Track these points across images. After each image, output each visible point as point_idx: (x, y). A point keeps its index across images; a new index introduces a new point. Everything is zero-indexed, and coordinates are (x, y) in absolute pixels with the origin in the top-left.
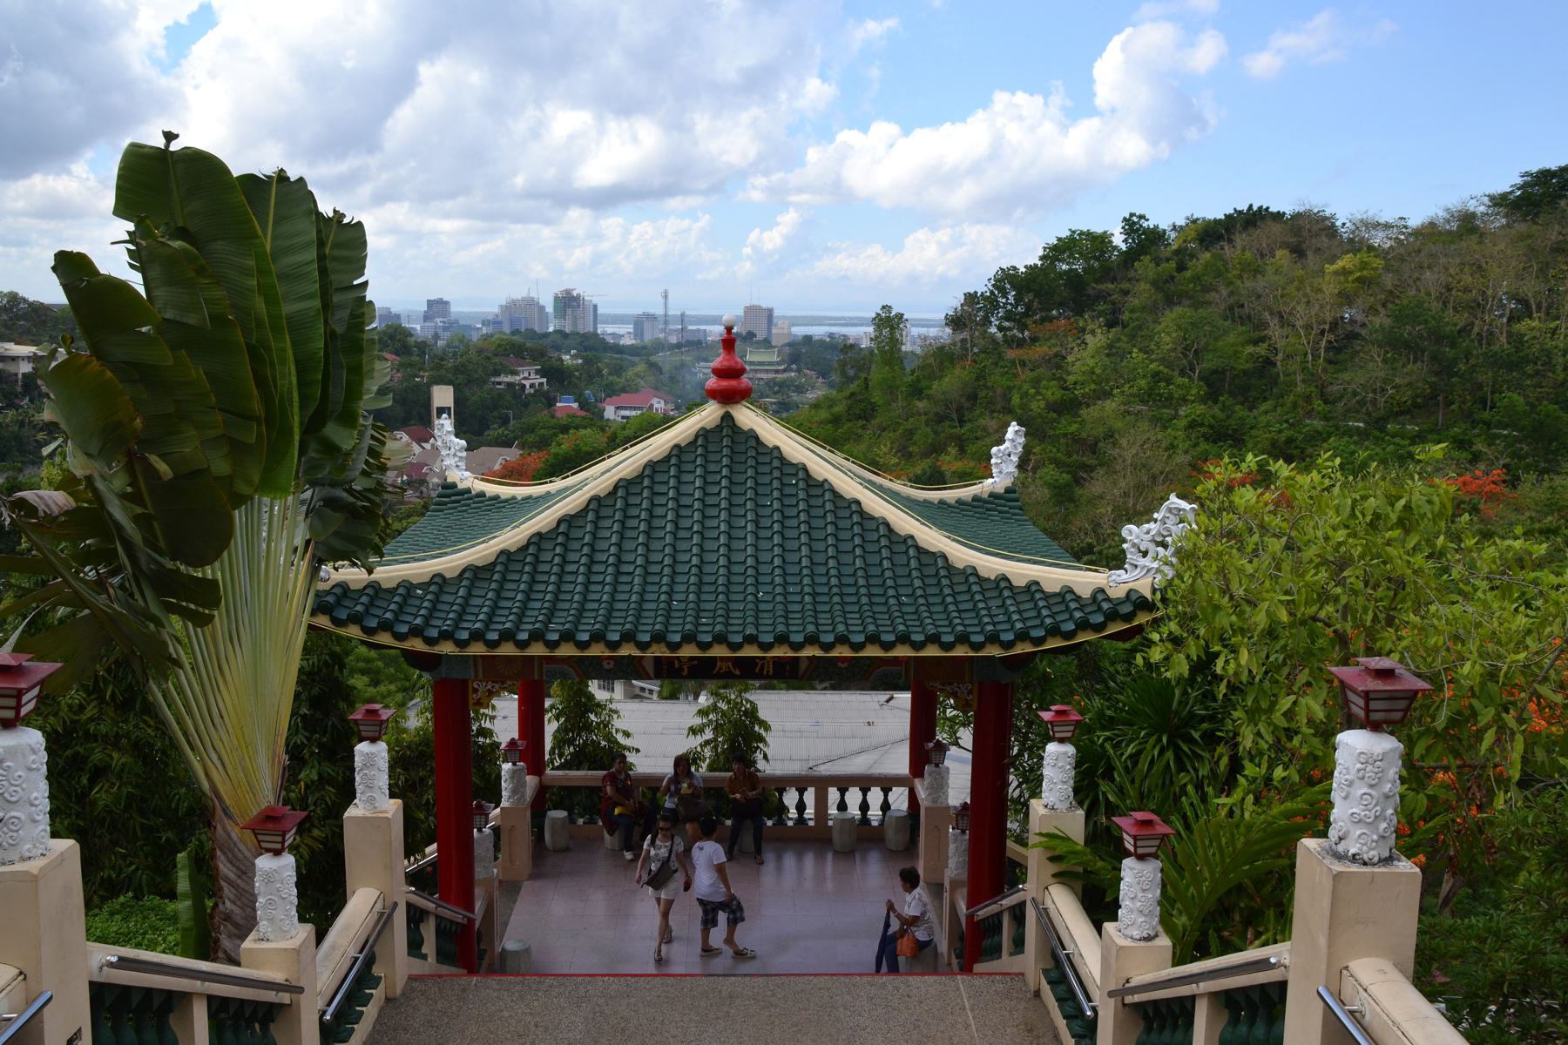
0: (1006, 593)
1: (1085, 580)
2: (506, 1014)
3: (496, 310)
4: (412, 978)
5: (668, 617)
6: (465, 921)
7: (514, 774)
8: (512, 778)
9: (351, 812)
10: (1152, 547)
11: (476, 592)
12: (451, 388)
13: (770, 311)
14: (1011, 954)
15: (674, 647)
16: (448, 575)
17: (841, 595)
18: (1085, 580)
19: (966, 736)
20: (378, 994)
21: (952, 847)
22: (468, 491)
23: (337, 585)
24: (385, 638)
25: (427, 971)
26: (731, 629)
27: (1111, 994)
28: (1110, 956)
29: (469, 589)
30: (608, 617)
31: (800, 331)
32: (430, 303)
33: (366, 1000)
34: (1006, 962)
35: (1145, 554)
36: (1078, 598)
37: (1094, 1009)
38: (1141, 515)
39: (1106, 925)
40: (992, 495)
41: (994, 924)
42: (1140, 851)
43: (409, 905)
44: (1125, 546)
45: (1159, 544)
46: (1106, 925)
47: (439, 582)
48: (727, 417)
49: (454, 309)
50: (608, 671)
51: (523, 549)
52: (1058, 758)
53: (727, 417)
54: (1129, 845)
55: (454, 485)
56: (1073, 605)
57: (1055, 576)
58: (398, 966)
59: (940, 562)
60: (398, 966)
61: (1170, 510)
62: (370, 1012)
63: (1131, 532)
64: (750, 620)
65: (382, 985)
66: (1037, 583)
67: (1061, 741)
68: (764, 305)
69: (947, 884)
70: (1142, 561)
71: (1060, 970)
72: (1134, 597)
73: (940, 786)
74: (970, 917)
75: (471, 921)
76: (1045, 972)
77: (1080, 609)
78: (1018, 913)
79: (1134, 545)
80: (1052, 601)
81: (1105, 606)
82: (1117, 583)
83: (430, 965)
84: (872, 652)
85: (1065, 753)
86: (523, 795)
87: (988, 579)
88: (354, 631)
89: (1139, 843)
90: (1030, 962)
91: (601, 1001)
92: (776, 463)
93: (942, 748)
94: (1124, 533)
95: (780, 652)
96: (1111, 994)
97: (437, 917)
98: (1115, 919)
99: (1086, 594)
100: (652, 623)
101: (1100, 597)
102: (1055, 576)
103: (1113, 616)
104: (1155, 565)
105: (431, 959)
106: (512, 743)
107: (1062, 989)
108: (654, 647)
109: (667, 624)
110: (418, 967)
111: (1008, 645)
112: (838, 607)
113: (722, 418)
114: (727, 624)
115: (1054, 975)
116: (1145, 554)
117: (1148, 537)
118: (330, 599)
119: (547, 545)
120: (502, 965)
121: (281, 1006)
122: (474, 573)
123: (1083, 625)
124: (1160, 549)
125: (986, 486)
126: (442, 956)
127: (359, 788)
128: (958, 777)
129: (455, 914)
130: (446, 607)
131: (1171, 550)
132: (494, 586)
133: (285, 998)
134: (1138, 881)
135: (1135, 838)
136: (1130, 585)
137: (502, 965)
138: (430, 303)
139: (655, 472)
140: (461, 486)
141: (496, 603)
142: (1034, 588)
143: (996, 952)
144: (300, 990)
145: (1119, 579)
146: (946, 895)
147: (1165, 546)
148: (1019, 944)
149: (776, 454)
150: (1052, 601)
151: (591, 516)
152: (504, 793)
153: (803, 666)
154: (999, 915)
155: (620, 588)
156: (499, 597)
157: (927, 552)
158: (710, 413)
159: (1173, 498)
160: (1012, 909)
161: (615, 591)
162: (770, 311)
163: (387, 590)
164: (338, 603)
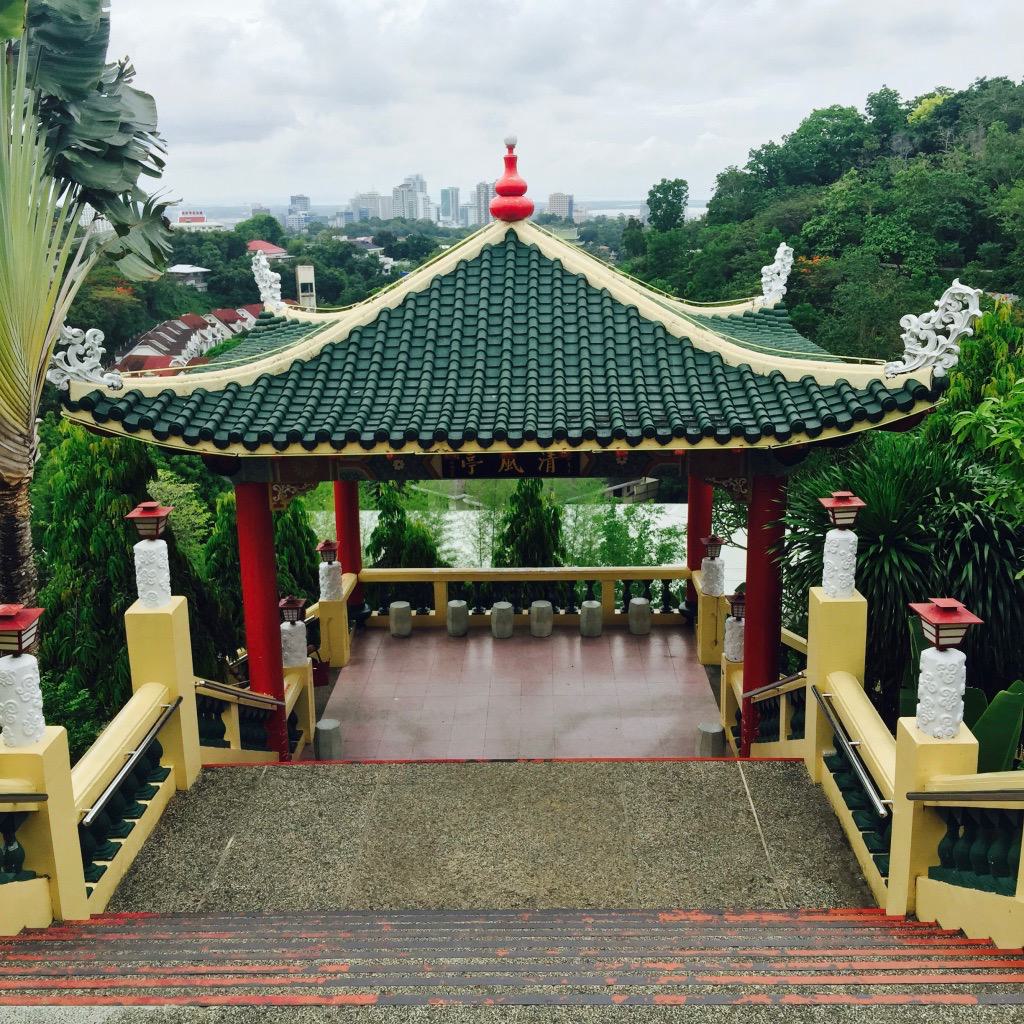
0: (782, 388)
1: (859, 374)
2: (292, 803)
3: (347, 203)
4: (206, 768)
5: (451, 418)
6: (275, 708)
7: (329, 572)
8: (328, 575)
9: (133, 610)
10: (932, 336)
11: (269, 399)
12: (312, 268)
13: (571, 197)
14: (790, 738)
15: (456, 445)
16: (243, 384)
17: (620, 394)
18: (859, 374)
19: (741, 536)
20: (165, 789)
21: (728, 635)
22: (284, 319)
23: (130, 393)
24: (176, 443)
25: (229, 761)
26: (511, 427)
27: (910, 796)
28: (908, 756)
29: (263, 396)
30: (395, 419)
31: (595, 213)
32: (294, 200)
33: (150, 794)
34: (784, 747)
35: (925, 343)
36: (854, 391)
37: (886, 806)
38: (921, 306)
39: (903, 721)
40: (764, 311)
41: (770, 709)
42: (942, 642)
43: (201, 700)
44: (903, 336)
45: (938, 332)
46: (903, 721)
47: (235, 390)
48: (511, 233)
49: (313, 203)
50: (398, 472)
51: (317, 359)
52: (841, 547)
53: (511, 233)
54: (929, 633)
55: (271, 315)
56: (850, 396)
57: (829, 370)
58: (189, 756)
59: (716, 362)
60: (189, 756)
61: (953, 296)
62: (154, 807)
63: (911, 322)
64: (530, 417)
65: (171, 776)
66: (812, 378)
67: (843, 527)
68: (566, 193)
69: (724, 667)
70: (921, 351)
71: (846, 765)
72: (912, 387)
73: (715, 576)
74: (747, 700)
75: (282, 708)
76: (827, 760)
77: (858, 400)
78: (797, 700)
79: (913, 335)
80: (827, 394)
81: (883, 396)
82: (890, 374)
83: (234, 751)
84: (649, 445)
85: (847, 540)
86: (339, 591)
87: (763, 376)
88: (146, 436)
89: (942, 633)
90: (808, 749)
91: (386, 789)
92: (558, 274)
93: (716, 543)
94: (903, 322)
95: (561, 447)
96: (910, 796)
97: (240, 706)
98: (912, 713)
99: (861, 385)
100: (437, 421)
101: (877, 387)
102: (829, 370)
103: (890, 406)
104: (936, 353)
105: (236, 745)
106: (328, 544)
107: (845, 778)
108: (437, 446)
109: (450, 424)
110: (214, 755)
111: (782, 437)
112: (616, 404)
113: (507, 235)
114: (508, 423)
115: (837, 763)
116: (925, 343)
117: (929, 326)
118: (122, 406)
119: (339, 355)
120: (319, 750)
121: (25, 814)
122: (269, 382)
123: (860, 416)
124: (941, 338)
125: (756, 304)
126: (247, 742)
127: (140, 586)
128: (732, 566)
129: (264, 699)
130: (239, 413)
131: (953, 337)
132: (287, 392)
133: (31, 807)
134: (941, 673)
135: (938, 627)
136: (909, 376)
137: (319, 750)
138: (294, 200)
139: (442, 285)
140: (277, 315)
141: (287, 408)
142: (809, 382)
143: (772, 734)
144: (42, 798)
145: (896, 371)
146: (723, 677)
147: (947, 334)
148: (797, 730)
149: (557, 266)
150: (827, 394)
151: (382, 327)
152: (322, 589)
153: (584, 462)
154: (776, 699)
155: (407, 392)
156: (291, 403)
157: (703, 354)
158: (495, 232)
159: (956, 282)
160: (790, 694)
161: (403, 395)
162: (571, 197)
163: (182, 399)
164: (130, 409)
